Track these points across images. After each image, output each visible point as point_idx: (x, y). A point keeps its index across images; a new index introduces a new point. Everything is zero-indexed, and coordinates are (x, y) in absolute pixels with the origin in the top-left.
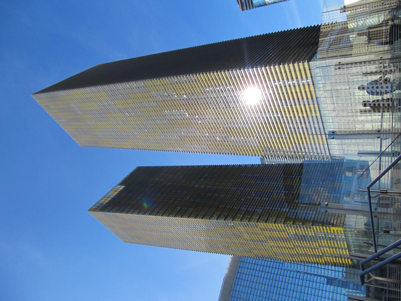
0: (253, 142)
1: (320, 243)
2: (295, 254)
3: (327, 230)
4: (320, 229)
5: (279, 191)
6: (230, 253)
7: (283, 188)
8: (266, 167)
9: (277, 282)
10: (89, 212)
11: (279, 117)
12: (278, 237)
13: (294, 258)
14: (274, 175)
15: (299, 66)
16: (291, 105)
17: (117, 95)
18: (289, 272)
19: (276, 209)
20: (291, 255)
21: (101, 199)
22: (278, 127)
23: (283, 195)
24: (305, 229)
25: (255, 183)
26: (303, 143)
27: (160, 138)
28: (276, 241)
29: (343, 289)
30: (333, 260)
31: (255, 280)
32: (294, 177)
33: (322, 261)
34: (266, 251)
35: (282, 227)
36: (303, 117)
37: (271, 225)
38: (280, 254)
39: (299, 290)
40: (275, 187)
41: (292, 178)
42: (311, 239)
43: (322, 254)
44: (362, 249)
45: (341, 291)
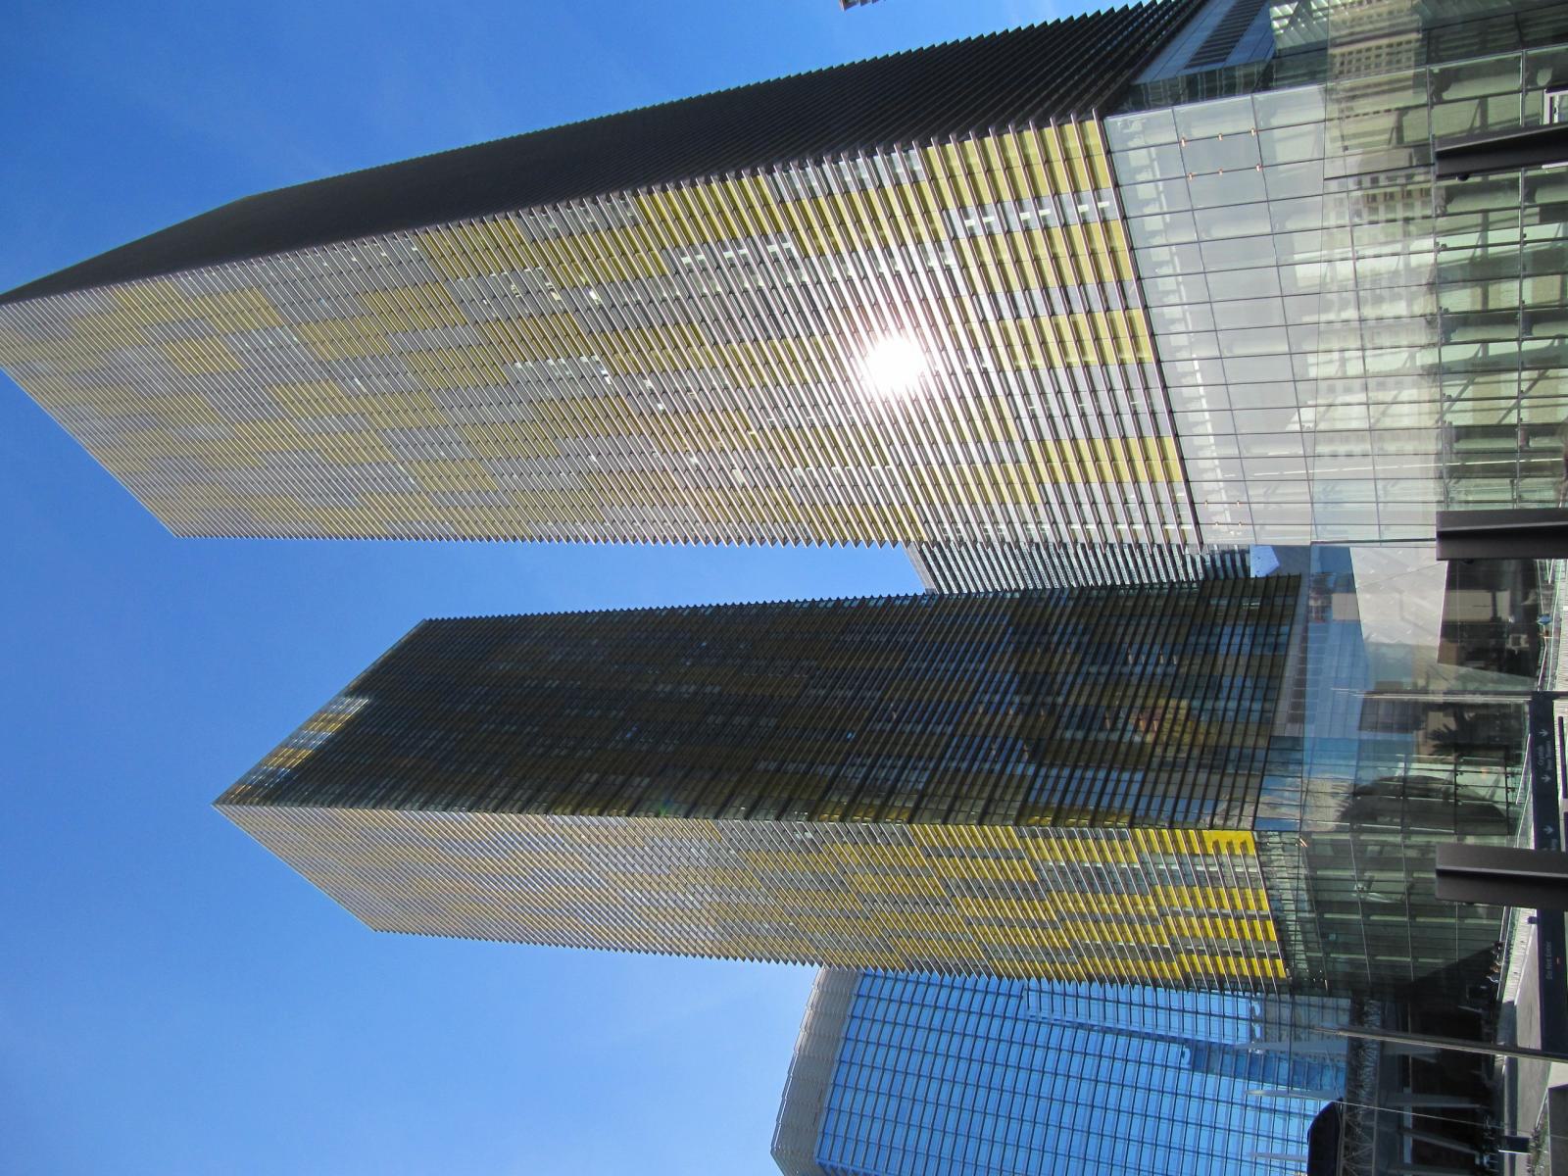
0: (881, 485)
1: (1162, 898)
2: (1066, 949)
3: (1188, 841)
4: (1161, 842)
5: (997, 698)
6: (806, 956)
7: (1014, 686)
8: (945, 606)
9: (999, 1070)
10: (217, 809)
11: (985, 372)
12: (997, 880)
13: (1063, 963)
14: (976, 632)
15: (1062, 138)
16: (1035, 317)
17: (310, 301)
18: (1044, 1029)
19: (987, 766)
20: (1047, 954)
21: (273, 755)
22: (985, 413)
23: (1011, 712)
24: (1103, 842)
25: (899, 669)
26: (1087, 482)
27: (500, 485)
28: (986, 897)
29: (1253, 1084)
30: (1215, 965)
31: (913, 1068)
32: (1056, 638)
33: (1172, 971)
34: (949, 940)
35: (1009, 837)
36: (1086, 366)
37: (965, 833)
38: (1005, 952)
39: (1085, 1096)
40: (980, 681)
41: (1049, 643)
42: (1127, 885)
43: (1173, 944)
44: (1327, 916)
45: (1246, 1093)
